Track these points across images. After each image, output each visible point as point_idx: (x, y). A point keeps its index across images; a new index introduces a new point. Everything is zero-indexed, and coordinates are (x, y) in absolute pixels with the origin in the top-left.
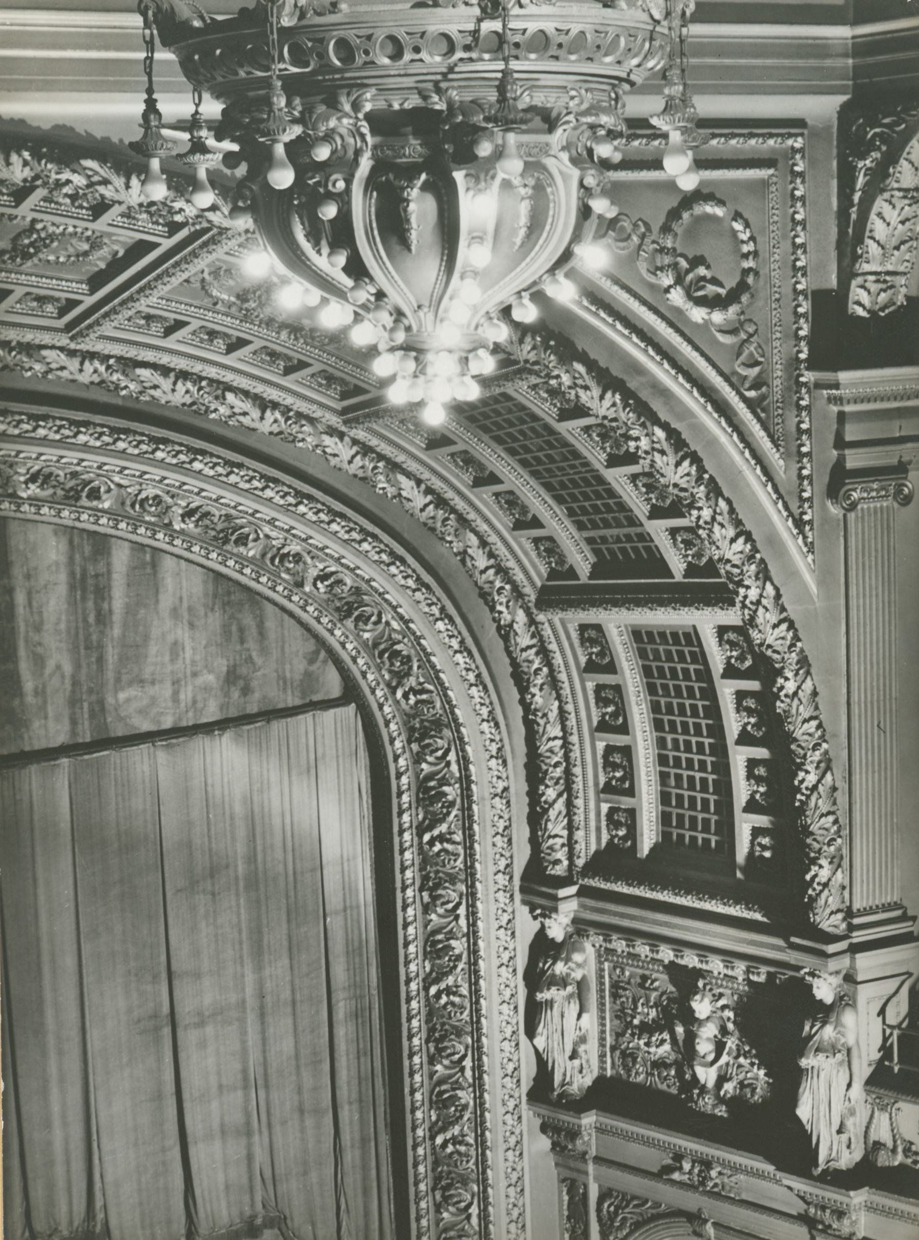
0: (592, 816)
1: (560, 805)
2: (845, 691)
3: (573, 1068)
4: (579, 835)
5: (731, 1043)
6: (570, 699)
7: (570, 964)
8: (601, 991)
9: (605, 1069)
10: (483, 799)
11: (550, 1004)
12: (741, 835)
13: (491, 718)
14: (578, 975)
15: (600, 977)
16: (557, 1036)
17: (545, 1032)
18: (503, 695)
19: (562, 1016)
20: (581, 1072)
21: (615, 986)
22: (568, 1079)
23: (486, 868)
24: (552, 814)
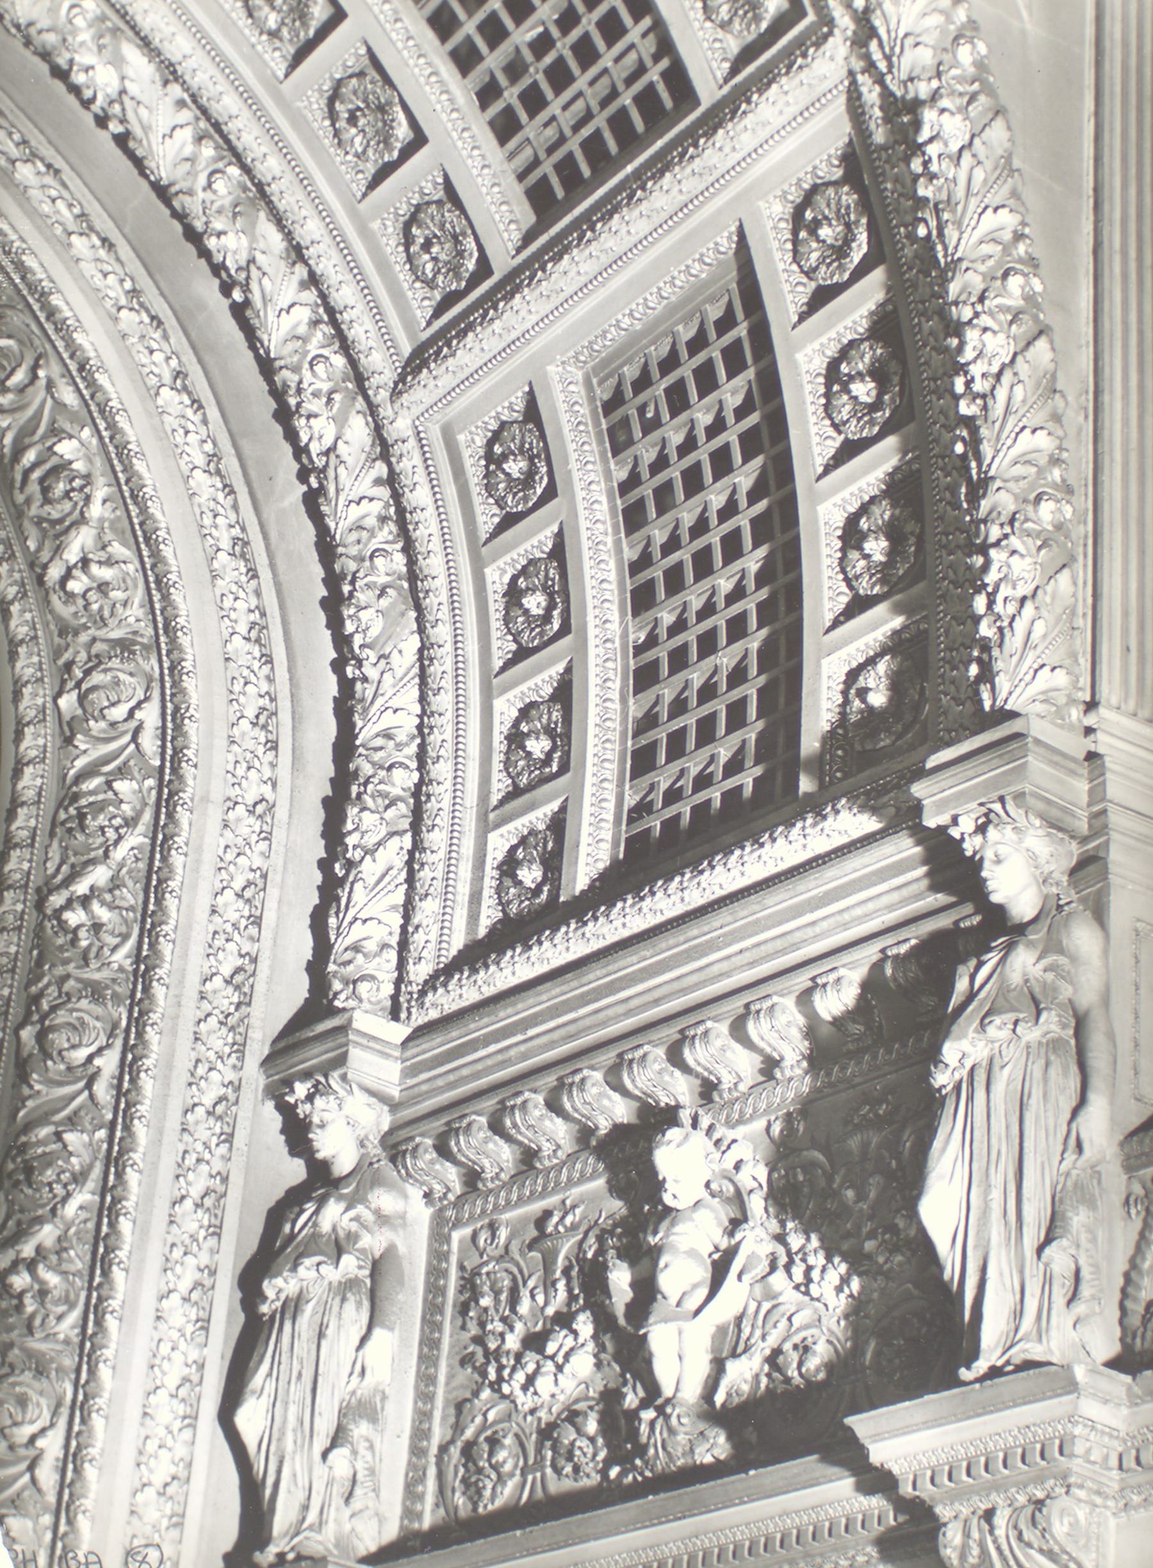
0: (465, 871)
1: (394, 853)
2: (1088, 227)
3: (330, 1483)
4: (427, 910)
5: (756, 1241)
6: (444, 614)
7: (360, 1209)
8: (434, 1289)
9: (419, 1516)
10: (206, 799)
11: (293, 1306)
12: (816, 692)
13: (264, 719)
14: (373, 1242)
15: (437, 1256)
16: (299, 1392)
17: (270, 1387)
18: (292, 618)
19: (321, 1335)
20: (348, 1498)
21: (470, 1285)
22: (312, 1517)
23: (185, 956)
24: (370, 869)
